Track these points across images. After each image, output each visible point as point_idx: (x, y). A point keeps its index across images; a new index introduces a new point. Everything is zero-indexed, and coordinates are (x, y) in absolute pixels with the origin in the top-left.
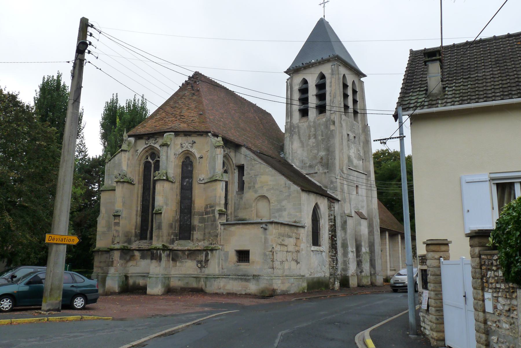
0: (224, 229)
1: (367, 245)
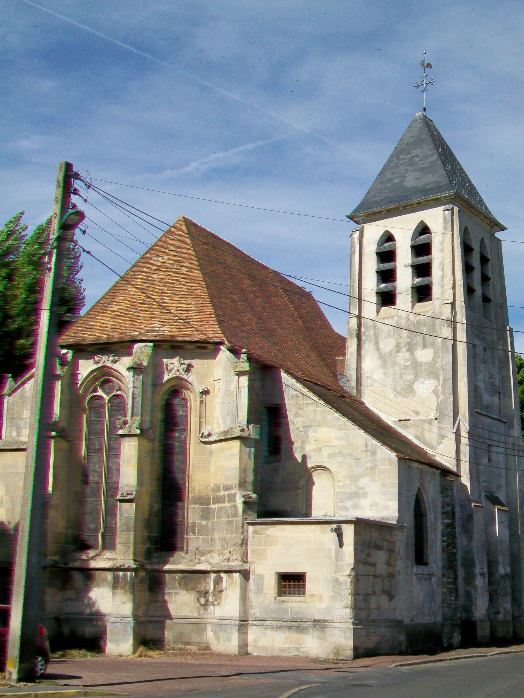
1: (507, 561)
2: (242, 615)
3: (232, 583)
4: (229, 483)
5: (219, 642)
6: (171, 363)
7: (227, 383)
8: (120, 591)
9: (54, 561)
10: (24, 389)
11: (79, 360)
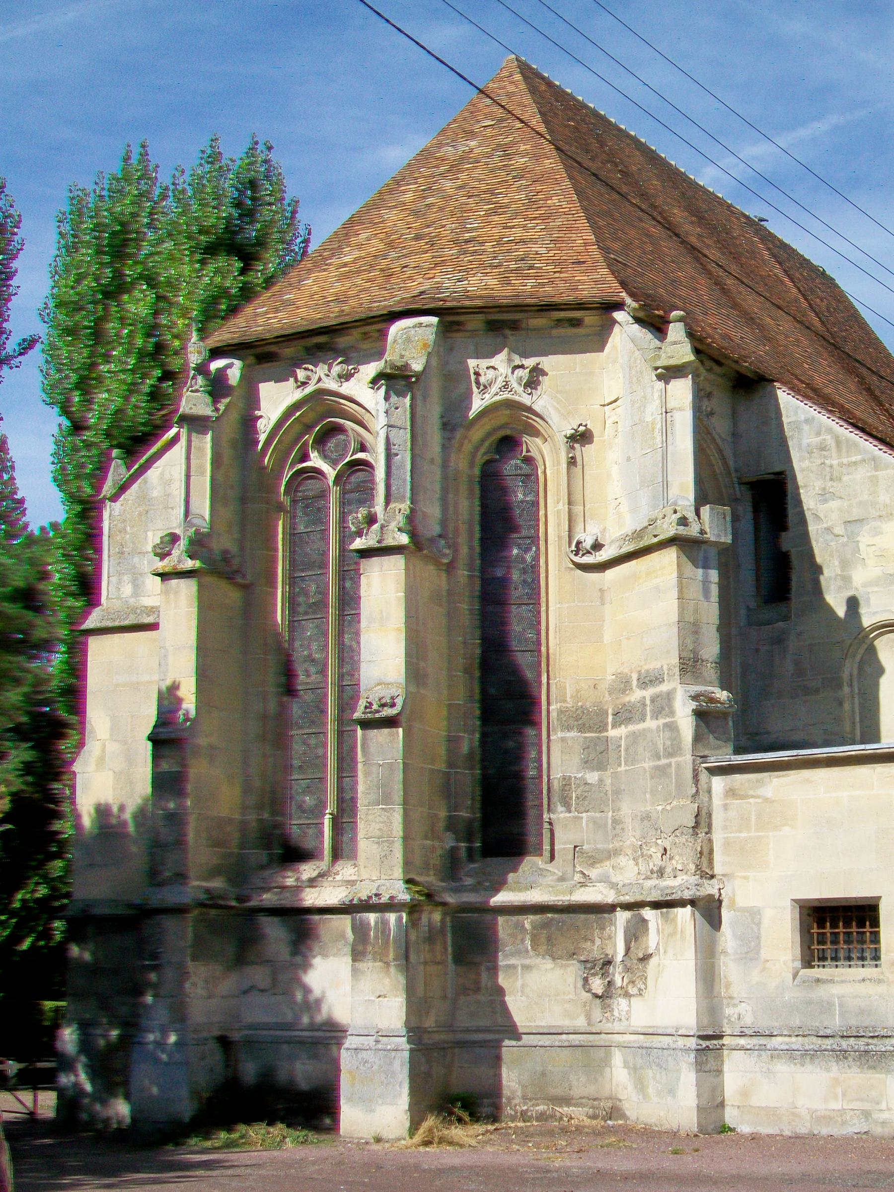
2: (705, 1021)
3: (672, 934)
4: (653, 665)
5: (646, 1097)
6: (487, 368)
7: (637, 405)
8: (370, 964)
9: (208, 891)
10: (146, 482)
11: (262, 386)
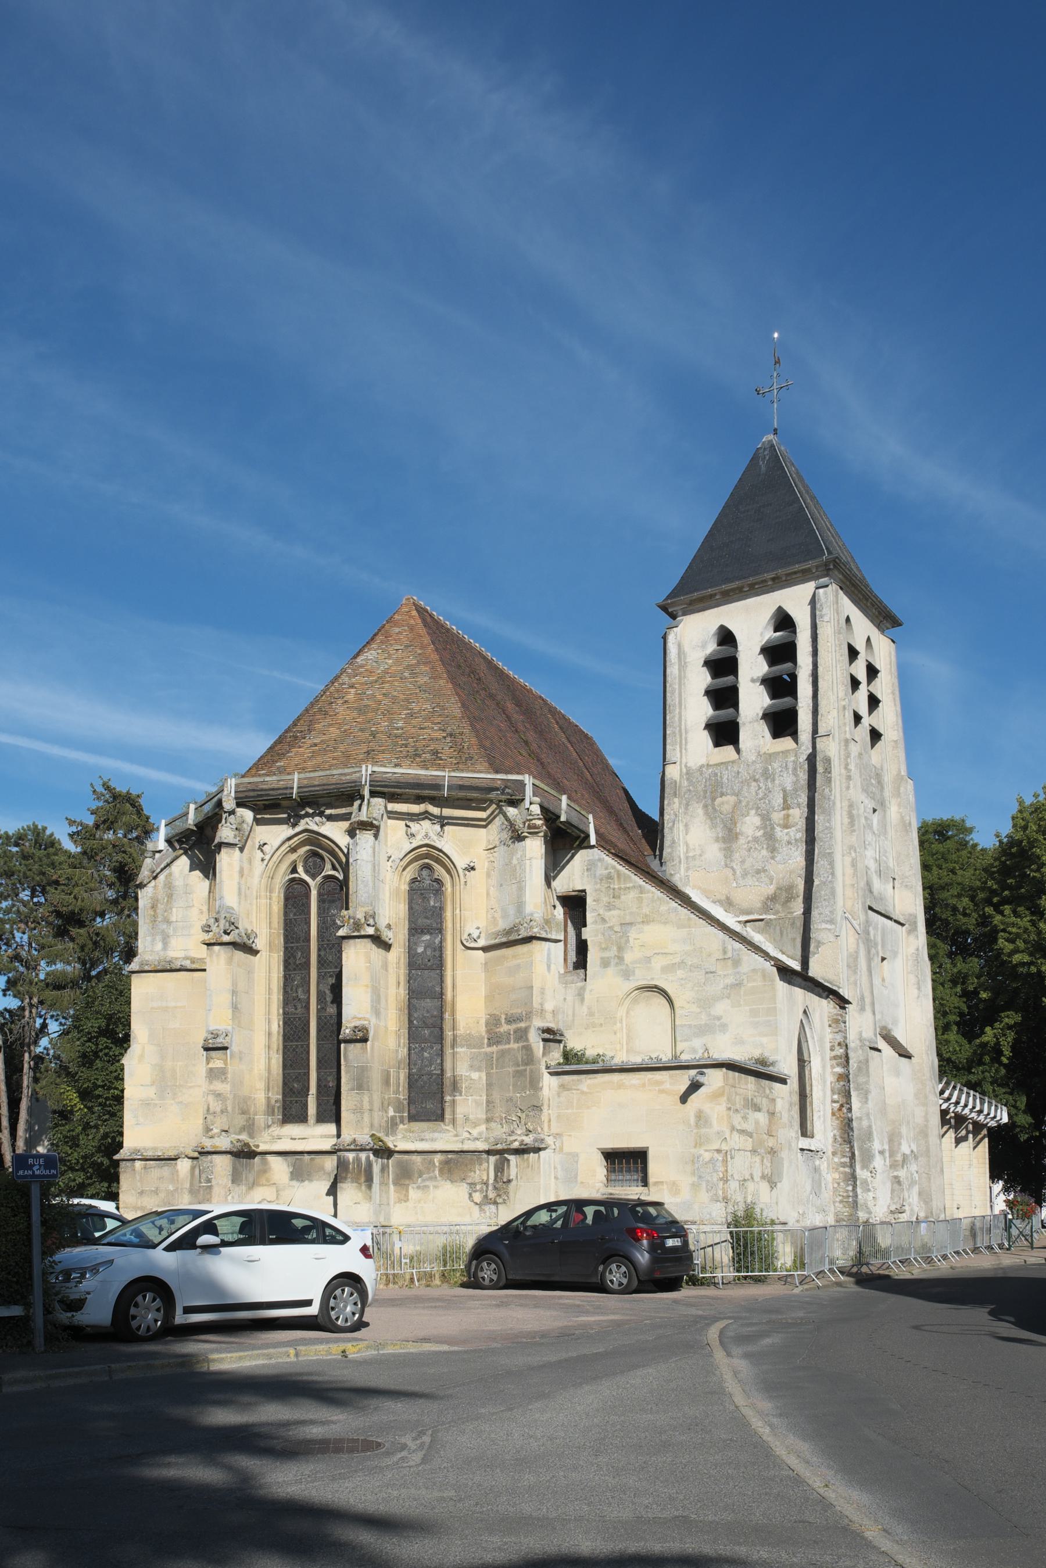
0: (563, 1087)
8: (349, 1184)
10: (170, 874)
